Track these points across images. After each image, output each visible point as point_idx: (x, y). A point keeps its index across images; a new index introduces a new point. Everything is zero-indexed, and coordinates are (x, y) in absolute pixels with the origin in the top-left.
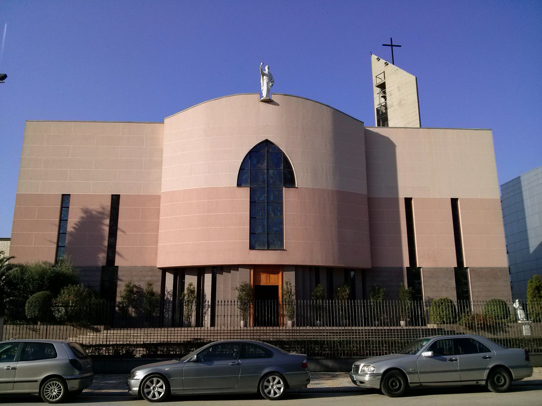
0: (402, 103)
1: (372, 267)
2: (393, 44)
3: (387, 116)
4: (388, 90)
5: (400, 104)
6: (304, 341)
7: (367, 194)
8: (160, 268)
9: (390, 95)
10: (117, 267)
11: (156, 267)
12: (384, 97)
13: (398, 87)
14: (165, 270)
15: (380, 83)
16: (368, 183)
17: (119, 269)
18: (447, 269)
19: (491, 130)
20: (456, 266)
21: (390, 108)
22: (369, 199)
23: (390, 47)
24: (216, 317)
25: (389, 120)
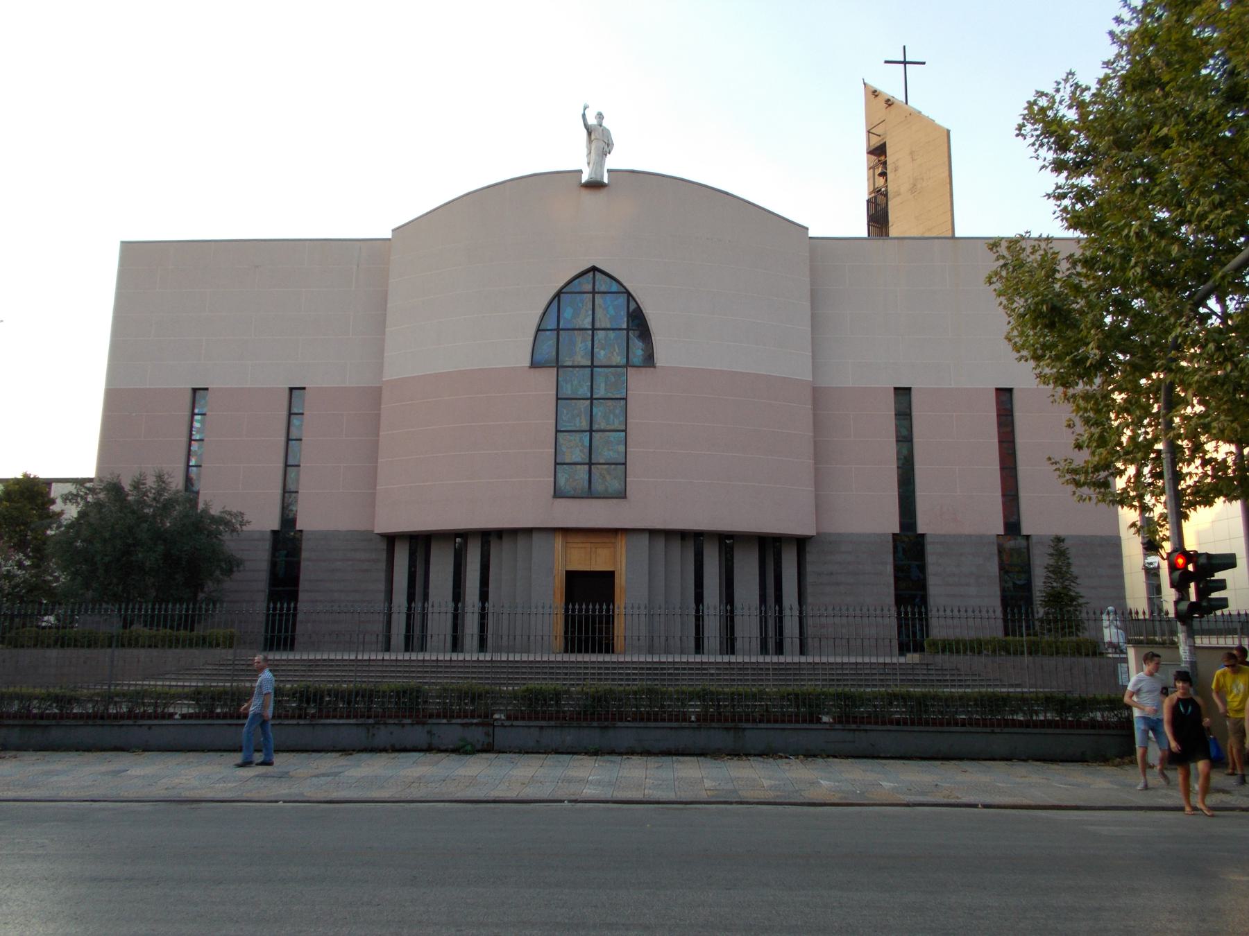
0: (919, 186)
1: (818, 534)
2: (907, 60)
3: (887, 212)
4: (890, 160)
5: (913, 188)
6: (226, 693)
7: (811, 379)
8: (383, 535)
9: (895, 171)
10: (923, 535)
11: (373, 531)
12: (883, 174)
13: (912, 153)
14: (391, 539)
15: (876, 146)
16: (813, 357)
17: (928, 540)
18: (981, 537)
19: (811, 238)
20: (897, 531)
21: (894, 197)
22: (815, 390)
23: (902, 65)
24: (429, 638)
25: (890, 224)
